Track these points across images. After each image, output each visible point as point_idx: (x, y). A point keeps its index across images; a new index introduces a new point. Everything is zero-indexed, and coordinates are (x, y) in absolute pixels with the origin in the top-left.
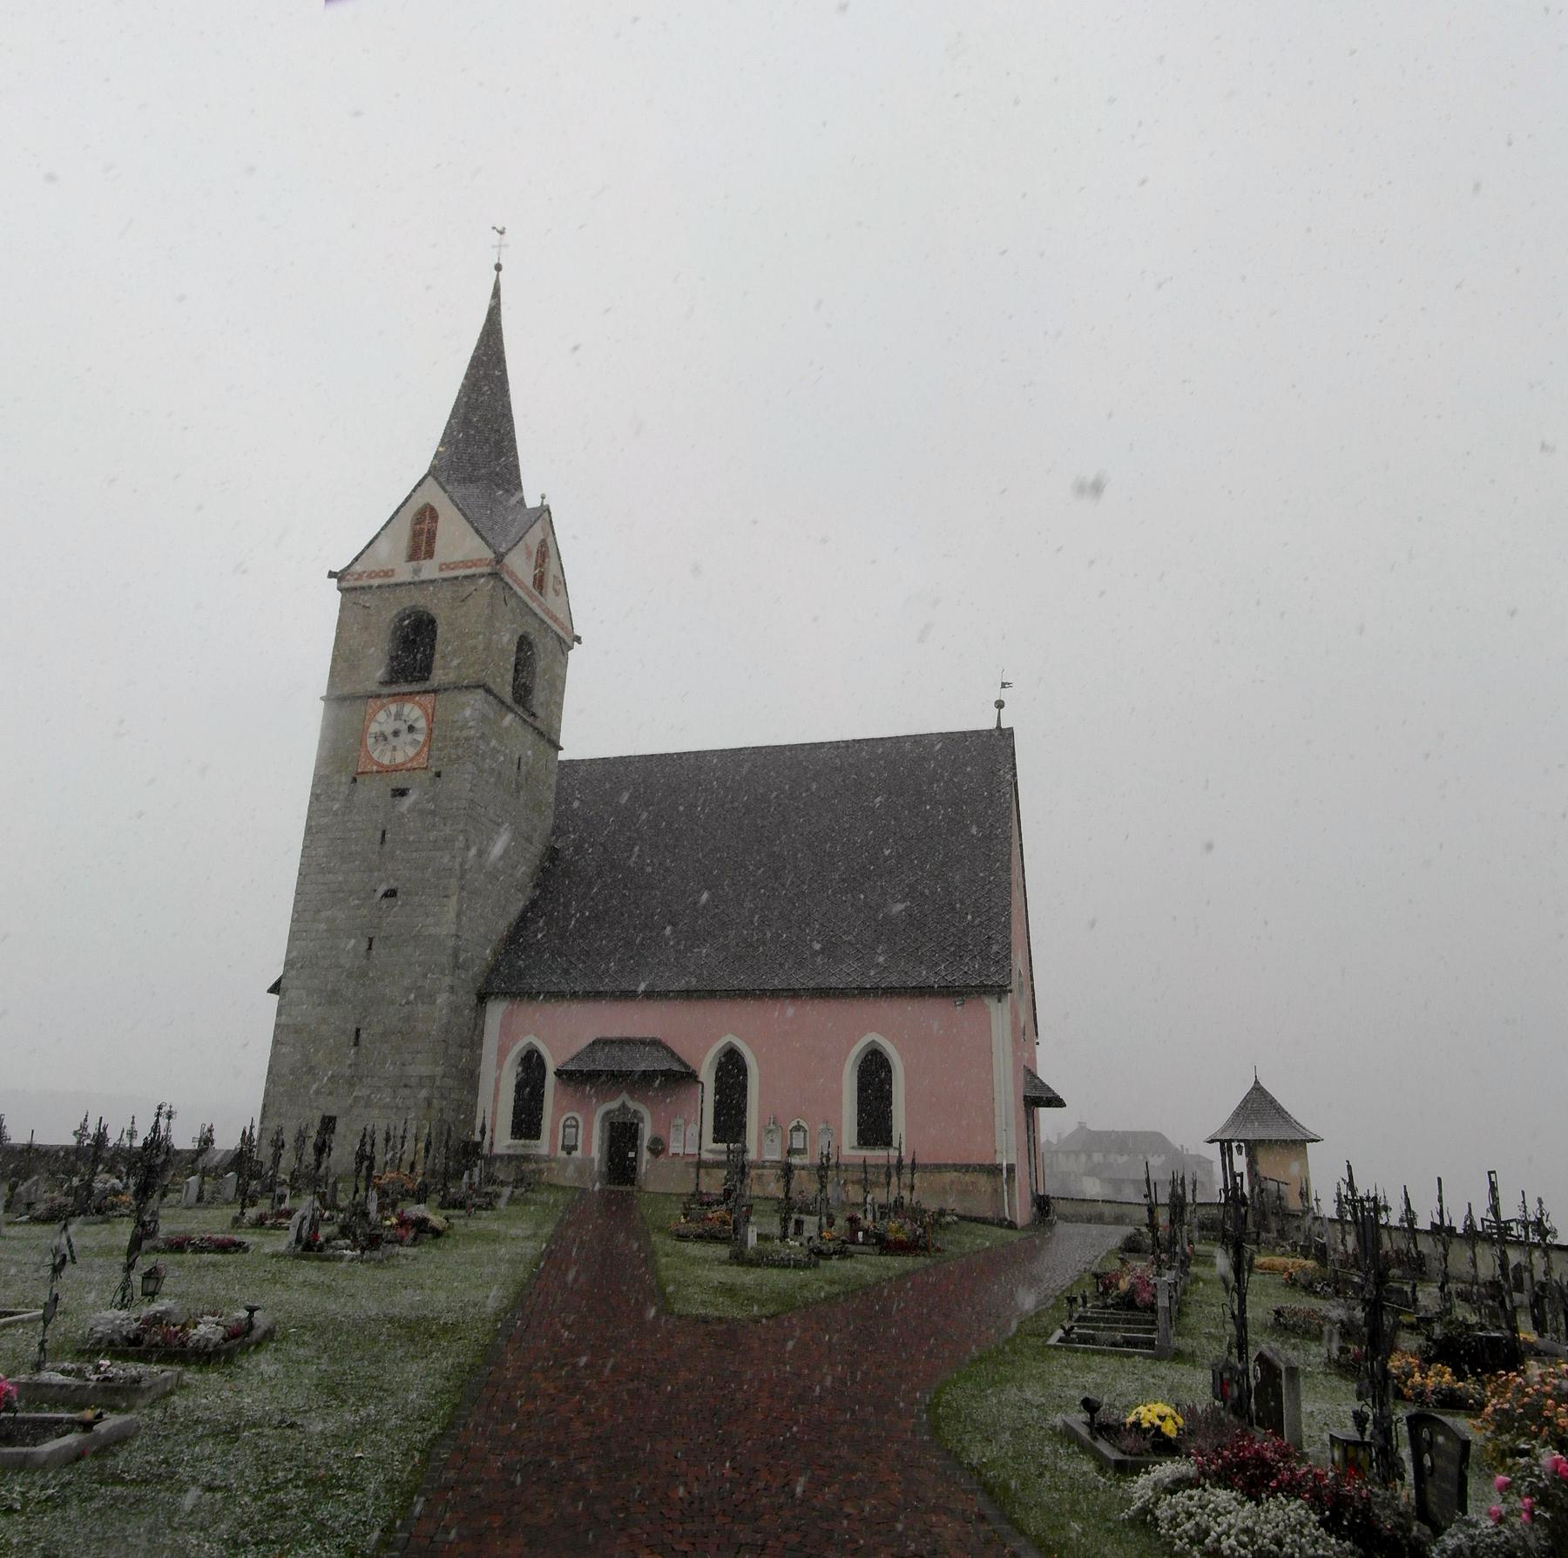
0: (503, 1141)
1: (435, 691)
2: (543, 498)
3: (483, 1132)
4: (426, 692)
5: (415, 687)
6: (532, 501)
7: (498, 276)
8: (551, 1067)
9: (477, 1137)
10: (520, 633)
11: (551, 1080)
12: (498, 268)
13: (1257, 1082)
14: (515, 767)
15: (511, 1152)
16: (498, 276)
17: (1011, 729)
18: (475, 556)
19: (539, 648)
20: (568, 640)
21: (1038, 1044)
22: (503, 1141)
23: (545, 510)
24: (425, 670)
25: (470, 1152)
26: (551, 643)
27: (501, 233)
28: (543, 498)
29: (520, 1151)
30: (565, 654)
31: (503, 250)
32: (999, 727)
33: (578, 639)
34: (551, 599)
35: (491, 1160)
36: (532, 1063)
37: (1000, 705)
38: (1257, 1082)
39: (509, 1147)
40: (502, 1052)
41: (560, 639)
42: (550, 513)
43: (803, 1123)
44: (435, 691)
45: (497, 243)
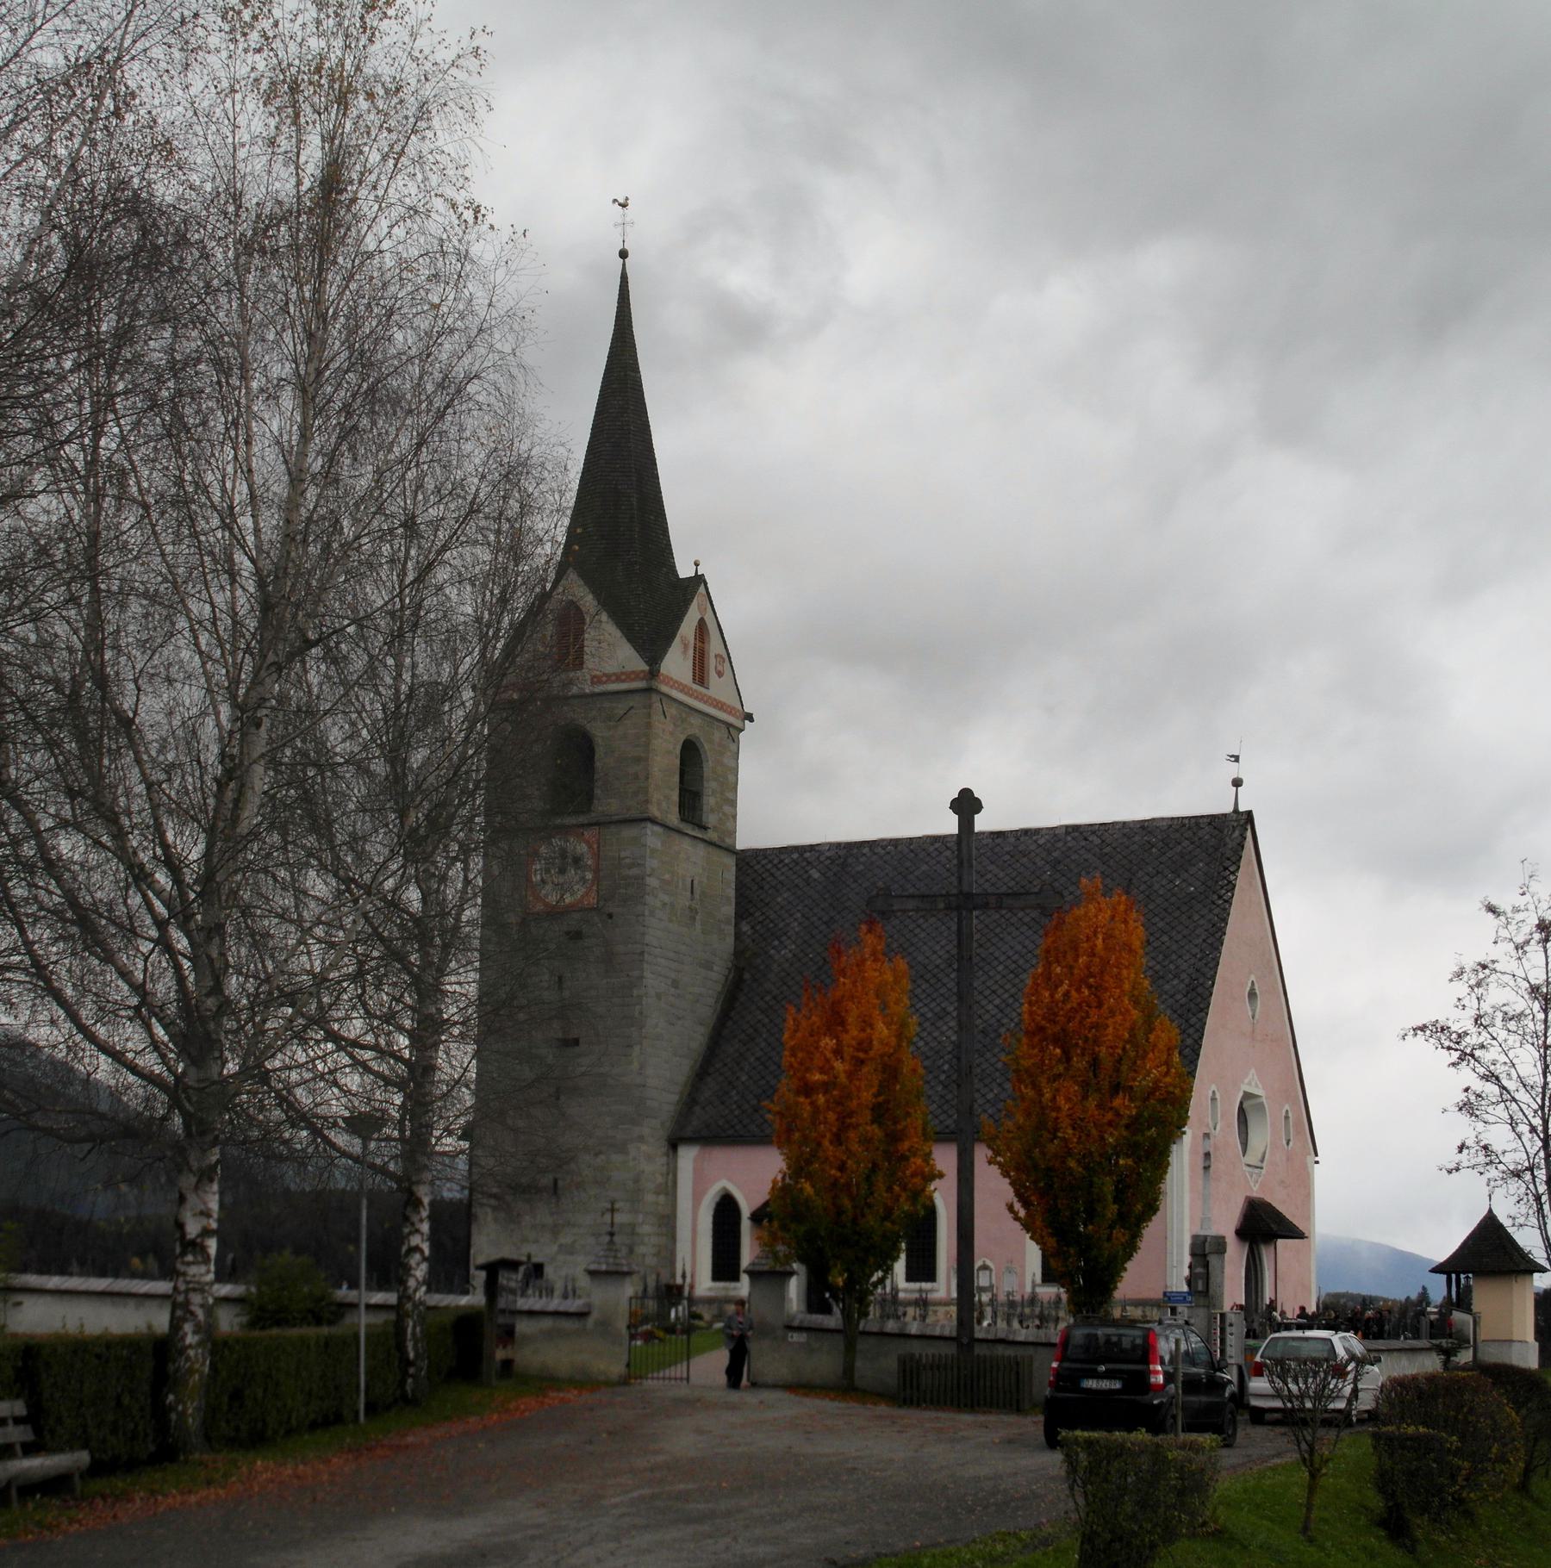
0: (704, 1284)
1: (597, 824)
2: (697, 564)
3: (684, 1276)
4: (590, 825)
5: (582, 819)
6: (684, 571)
7: (624, 265)
8: (746, 1211)
9: (679, 1281)
10: (683, 738)
11: (746, 1225)
12: (623, 254)
13: (1490, 1211)
14: (689, 893)
15: (712, 1294)
16: (624, 265)
17: (1249, 813)
18: (629, 668)
19: (707, 748)
20: (737, 723)
21: (1317, 1162)
22: (704, 1284)
23: (699, 580)
24: (586, 800)
25: (672, 1293)
26: (719, 734)
27: (624, 206)
28: (697, 564)
29: (722, 1293)
30: (736, 741)
31: (628, 228)
32: (1236, 811)
33: (750, 717)
34: (717, 688)
35: (692, 1300)
36: (726, 1210)
37: (1237, 783)
38: (1490, 1211)
39: (710, 1289)
40: (697, 1198)
41: (729, 725)
42: (706, 584)
43: (989, 1263)
44: (597, 824)
45: (620, 221)
